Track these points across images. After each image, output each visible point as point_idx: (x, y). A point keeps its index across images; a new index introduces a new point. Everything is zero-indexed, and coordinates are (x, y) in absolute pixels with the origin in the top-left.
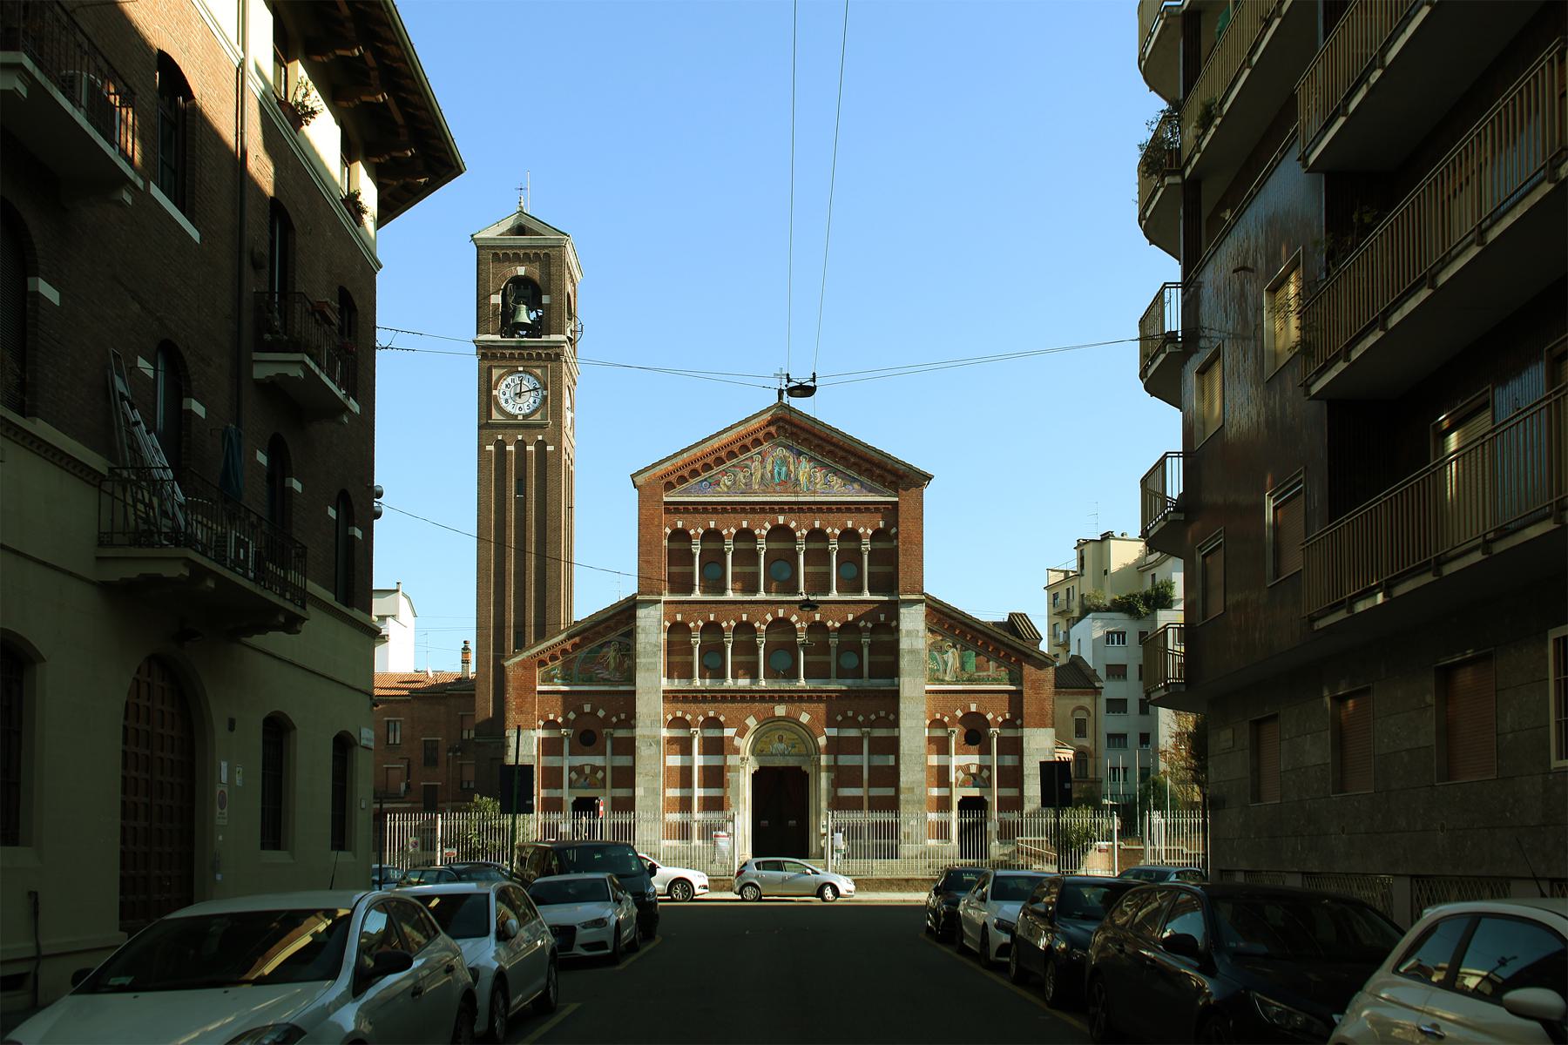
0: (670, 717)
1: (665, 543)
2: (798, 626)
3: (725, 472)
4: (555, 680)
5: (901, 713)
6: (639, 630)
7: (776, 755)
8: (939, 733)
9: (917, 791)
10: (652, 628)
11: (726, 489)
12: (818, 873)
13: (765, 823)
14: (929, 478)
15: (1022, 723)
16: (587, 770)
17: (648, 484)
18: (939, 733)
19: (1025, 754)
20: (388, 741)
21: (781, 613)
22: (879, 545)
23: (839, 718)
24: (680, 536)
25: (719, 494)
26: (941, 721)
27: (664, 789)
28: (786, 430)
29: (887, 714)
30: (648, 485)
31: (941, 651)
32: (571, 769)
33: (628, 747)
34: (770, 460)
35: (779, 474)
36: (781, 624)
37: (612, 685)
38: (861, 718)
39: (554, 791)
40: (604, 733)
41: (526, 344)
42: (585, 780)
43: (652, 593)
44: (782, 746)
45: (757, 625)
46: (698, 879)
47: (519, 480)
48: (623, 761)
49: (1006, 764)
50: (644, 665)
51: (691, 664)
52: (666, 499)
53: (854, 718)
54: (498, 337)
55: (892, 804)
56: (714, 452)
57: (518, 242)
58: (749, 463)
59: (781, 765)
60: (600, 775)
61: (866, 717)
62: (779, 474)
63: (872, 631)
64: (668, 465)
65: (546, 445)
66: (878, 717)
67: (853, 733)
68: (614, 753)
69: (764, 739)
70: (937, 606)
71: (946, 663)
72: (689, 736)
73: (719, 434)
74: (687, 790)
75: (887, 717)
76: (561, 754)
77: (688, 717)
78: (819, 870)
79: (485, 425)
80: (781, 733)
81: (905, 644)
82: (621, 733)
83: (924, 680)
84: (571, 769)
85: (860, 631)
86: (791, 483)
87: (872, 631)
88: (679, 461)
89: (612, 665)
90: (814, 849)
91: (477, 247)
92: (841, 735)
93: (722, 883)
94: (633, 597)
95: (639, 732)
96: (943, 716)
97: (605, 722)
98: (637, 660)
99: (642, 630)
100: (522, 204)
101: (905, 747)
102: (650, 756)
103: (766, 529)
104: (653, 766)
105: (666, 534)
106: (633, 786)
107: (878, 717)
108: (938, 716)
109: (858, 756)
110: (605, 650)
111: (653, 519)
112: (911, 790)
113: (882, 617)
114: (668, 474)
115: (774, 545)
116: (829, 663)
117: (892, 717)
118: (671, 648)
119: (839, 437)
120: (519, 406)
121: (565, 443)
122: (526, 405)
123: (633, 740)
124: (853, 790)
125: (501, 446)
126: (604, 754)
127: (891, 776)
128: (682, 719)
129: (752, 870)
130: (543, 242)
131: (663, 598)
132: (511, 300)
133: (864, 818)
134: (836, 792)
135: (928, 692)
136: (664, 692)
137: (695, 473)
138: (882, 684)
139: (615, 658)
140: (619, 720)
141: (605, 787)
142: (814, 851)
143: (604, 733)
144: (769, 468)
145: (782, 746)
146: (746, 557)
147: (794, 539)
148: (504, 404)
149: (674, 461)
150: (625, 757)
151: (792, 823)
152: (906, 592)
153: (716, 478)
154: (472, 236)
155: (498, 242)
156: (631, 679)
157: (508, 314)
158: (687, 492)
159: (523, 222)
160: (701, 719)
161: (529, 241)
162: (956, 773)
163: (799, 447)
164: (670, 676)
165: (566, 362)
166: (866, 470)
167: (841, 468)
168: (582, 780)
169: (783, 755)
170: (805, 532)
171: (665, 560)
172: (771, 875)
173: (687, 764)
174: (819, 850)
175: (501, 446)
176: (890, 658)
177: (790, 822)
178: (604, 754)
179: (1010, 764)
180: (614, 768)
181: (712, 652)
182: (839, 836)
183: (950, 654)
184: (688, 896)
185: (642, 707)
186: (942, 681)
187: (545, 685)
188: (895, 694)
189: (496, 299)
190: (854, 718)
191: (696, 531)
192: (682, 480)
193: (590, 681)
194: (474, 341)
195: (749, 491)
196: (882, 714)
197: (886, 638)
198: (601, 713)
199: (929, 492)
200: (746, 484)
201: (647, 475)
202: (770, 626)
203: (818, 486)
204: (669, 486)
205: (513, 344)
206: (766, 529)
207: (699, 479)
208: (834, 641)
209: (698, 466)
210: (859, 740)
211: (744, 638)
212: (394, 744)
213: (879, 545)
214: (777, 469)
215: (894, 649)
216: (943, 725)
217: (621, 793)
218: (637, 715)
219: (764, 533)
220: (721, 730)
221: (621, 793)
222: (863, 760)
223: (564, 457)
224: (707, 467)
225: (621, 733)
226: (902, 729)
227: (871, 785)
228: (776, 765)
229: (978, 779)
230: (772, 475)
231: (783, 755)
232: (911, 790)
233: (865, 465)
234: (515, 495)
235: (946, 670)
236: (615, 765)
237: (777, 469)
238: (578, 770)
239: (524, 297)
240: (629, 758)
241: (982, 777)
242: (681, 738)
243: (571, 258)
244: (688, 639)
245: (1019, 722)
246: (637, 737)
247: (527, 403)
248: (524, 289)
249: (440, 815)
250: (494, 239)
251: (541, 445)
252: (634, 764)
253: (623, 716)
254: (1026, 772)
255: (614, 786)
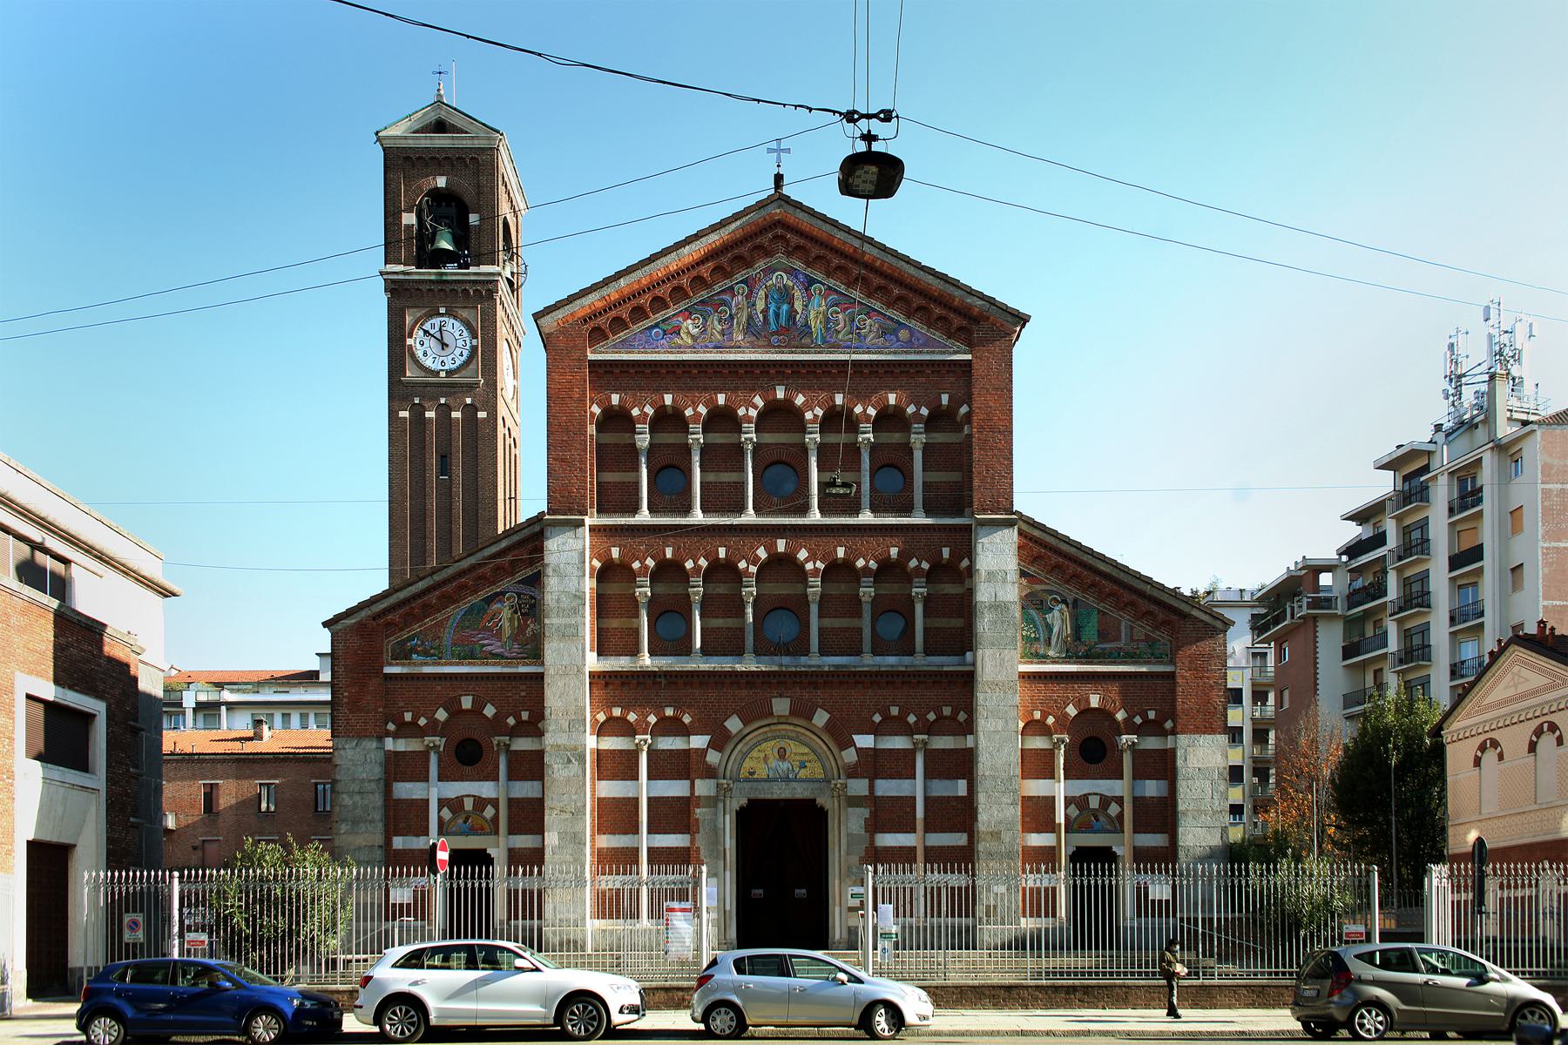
0: (601, 717)
1: (591, 429)
2: (809, 566)
3: (688, 313)
4: (414, 656)
5: (980, 708)
6: (549, 571)
7: (775, 780)
8: (1039, 743)
9: (1006, 837)
10: (569, 568)
11: (690, 341)
12: (859, 981)
13: (758, 892)
14: (1023, 320)
15: (1175, 726)
16: (468, 805)
17: (563, 331)
18: (1039, 743)
19: (1180, 777)
20: (316, 807)
21: (781, 545)
22: (940, 438)
23: (877, 718)
24: (615, 420)
25: (680, 348)
26: (1042, 722)
27: (593, 835)
28: (787, 241)
29: (955, 712)
30: (562, 333)
31: (1043, 608)
32: (442, 803)
33: (532, 766)
34: (762, 293)
35: (777, 315)
36: (782, 566)
37: (508, 665)
38: (912, 719)
39: (414, 839)
40: (495, 743)
41: (449, 278)
42: (465, 822)
43: (570, 511)
44: (785, 766)
45: (742, 565)
46: (618, 992)
47: (442, 456)
48: (525, 789)
49: (1147, 794)
50: (558, 630)
51: (636, 632)
52: (591, 357)
53: (902, 718)
54: (413, 269)
55: (964, 858)
56: (670, 277)
57: (437, 142)
58: (727, 297)
59: (783, 796)
60: (489, 812)
61: (921, 718)
62: (777, 315)
63: (931, 576)
64: (592, 298)
65: (477, 410)
66: (940, 717)
67: (899, 743)
68: (512, 777)
69: (754, 754)
70: (1036, 533)
71: (1049, 628)
72: (633, 748)
73: (679, 245)
74: (630, 836)
75: (953, 718)
76: (426, 779)
77: (632, 717)
78: (862, 974)
79: (399, 390)
80: (783, 743)
81: (984, 594)
82: (523, 744)
83: (1016, 654)
84: (442, 803)
85: (907, 577)
86: (793, 332)
87: (931, 576)
88: (612, 292)
89: (507, 632)
90: (837, 932)
91: (384, 150)
92: (881, 746)
93: (680, 994)
94: (539, 518)
95: (550, 739)
96: (1045, 715)
97: (497, 725)
98: (547, 621)
99: (554, 570)
100: (442, 92)
101: (986, 764)
102: (568, 780)
103: (755, 407)
104: (574, 797)
105: (592, 414)
106: (540, 830)
107: (940, 717)
108: (1037, 715)
109: (907, 781)
110: (495, 606)
111: (571, 389)
112: (996, 835)
113: (946, 552)
114: (595, 314)
115: (769, 438)
116: (859, 630)
117: (962, 717)
118: (603, 606)
119: (875, 252)
120: (441, 359)
121: (502, 411)
122: (450, 357)
123: (540, 754)
124: (899, 836)
125: (418, 412)
126: (496, 779)
127: (961, 814)
128: (622, 720)
129: (727, 975)
130: (469, 142)
131: (588, 521)
132: (428, 221)
133: (923, 878)
134: (872, 840)
135: (1025, 676)
136: (592, 675)
137: (639, 313)
138: (947, 663)
139: (511, 620)
140: (519, 722)
141: (497, 833)
142: (837, 936)
143: (495, 743)
144: (760, 305)
145: (785, 766)
146: (723, 457)
147: (801, 427)
148: (421, 356)
149: (605, 292)
150: (529, 784)
151: (801, 892)
152: (984, 511)
153: (674, 322)
154: (377, 133)
155: (411, 142)
156: (537, 655)
157: (424, 237)
158: (626, 345)
159: (443, 115)
160: (652, 719)
161: (450, 142)
162: (1066, 808)
163: (809, 271)
164: (602, 652)
165: (502, 303)
166: (920, 308)
167: (877, 306)
168: (460, 821)
169: (787, 779)
170: (819, 412)
171: (591, 459)
172: (765, 985)
173: (630, 795)
174: (845, 935)
175: (418, 412)
176: (957, 622)
177: (797, 891)
178: (496, 779)
179: (1154, 795)
180: (511, 802)
181: (669, 611)
182: (887, 909)
183: (1056, 613)
184: (597, 1029)
185: (554, 699)
186: (1043, 658)
187: (397, 665)
188: (968, 680)
189: (409, 219)
190: (902, 718)
191: (642, 411)
192: (619, 324)
193: (470, 656)
194: (382, 274)
195: (728, 344)
196: (947, 711)
197: (950, 589)
198: (489, 711)
199: (1026, 353)
200: (723, 333)
201: (560, 314)
202: (764, 568)
203: (840, 336)
204: (598, 335)
205: (433, 278)
206: (755, 407)
207: (647, 323)
208: (867, 591)
209: (644, 300)
210: (909, 755)
211: (721, 589)
212: (324, 811)
213: (940, 438)
214: (772, 308)
215: (965, 607)
216: (1046, 731)
217: (523, 841)
218: (547, 712)
219: (753, 413)
220: (686, 738)
221: (523, 841)
222: (916, 787)
223: (501, 430)
224: (659, 303)
225: (523, 744)
226: (981, 734)
227: (930, 827)
228: (775, 797)
229: (1102, 819)
230: (765, 318)
231: (787, 779)
232: (996, 835)
233: (918, 301)
234: (437, 477)
235: (1050, 639)
236: (513, 795)
237: (772, 308)
238: (455, 805)
239: (447, 218)
240: (537, 784)
241: (1108, 816)
242: (621, 751)
243: (505, 166)
244: (631, 592)
245: (1169, 725)
246: (548, 749)
247: (456, 356)
248: (446, 206)
249: (176, 874)
250: (406, 138)
251: (470, 411)
252: (543, 795)
253: (525, 716)
254: (1181, 807)
255: (511, 832)
